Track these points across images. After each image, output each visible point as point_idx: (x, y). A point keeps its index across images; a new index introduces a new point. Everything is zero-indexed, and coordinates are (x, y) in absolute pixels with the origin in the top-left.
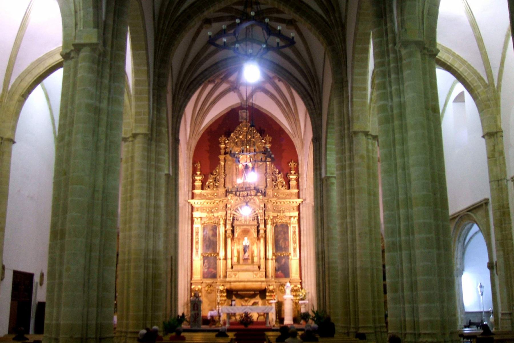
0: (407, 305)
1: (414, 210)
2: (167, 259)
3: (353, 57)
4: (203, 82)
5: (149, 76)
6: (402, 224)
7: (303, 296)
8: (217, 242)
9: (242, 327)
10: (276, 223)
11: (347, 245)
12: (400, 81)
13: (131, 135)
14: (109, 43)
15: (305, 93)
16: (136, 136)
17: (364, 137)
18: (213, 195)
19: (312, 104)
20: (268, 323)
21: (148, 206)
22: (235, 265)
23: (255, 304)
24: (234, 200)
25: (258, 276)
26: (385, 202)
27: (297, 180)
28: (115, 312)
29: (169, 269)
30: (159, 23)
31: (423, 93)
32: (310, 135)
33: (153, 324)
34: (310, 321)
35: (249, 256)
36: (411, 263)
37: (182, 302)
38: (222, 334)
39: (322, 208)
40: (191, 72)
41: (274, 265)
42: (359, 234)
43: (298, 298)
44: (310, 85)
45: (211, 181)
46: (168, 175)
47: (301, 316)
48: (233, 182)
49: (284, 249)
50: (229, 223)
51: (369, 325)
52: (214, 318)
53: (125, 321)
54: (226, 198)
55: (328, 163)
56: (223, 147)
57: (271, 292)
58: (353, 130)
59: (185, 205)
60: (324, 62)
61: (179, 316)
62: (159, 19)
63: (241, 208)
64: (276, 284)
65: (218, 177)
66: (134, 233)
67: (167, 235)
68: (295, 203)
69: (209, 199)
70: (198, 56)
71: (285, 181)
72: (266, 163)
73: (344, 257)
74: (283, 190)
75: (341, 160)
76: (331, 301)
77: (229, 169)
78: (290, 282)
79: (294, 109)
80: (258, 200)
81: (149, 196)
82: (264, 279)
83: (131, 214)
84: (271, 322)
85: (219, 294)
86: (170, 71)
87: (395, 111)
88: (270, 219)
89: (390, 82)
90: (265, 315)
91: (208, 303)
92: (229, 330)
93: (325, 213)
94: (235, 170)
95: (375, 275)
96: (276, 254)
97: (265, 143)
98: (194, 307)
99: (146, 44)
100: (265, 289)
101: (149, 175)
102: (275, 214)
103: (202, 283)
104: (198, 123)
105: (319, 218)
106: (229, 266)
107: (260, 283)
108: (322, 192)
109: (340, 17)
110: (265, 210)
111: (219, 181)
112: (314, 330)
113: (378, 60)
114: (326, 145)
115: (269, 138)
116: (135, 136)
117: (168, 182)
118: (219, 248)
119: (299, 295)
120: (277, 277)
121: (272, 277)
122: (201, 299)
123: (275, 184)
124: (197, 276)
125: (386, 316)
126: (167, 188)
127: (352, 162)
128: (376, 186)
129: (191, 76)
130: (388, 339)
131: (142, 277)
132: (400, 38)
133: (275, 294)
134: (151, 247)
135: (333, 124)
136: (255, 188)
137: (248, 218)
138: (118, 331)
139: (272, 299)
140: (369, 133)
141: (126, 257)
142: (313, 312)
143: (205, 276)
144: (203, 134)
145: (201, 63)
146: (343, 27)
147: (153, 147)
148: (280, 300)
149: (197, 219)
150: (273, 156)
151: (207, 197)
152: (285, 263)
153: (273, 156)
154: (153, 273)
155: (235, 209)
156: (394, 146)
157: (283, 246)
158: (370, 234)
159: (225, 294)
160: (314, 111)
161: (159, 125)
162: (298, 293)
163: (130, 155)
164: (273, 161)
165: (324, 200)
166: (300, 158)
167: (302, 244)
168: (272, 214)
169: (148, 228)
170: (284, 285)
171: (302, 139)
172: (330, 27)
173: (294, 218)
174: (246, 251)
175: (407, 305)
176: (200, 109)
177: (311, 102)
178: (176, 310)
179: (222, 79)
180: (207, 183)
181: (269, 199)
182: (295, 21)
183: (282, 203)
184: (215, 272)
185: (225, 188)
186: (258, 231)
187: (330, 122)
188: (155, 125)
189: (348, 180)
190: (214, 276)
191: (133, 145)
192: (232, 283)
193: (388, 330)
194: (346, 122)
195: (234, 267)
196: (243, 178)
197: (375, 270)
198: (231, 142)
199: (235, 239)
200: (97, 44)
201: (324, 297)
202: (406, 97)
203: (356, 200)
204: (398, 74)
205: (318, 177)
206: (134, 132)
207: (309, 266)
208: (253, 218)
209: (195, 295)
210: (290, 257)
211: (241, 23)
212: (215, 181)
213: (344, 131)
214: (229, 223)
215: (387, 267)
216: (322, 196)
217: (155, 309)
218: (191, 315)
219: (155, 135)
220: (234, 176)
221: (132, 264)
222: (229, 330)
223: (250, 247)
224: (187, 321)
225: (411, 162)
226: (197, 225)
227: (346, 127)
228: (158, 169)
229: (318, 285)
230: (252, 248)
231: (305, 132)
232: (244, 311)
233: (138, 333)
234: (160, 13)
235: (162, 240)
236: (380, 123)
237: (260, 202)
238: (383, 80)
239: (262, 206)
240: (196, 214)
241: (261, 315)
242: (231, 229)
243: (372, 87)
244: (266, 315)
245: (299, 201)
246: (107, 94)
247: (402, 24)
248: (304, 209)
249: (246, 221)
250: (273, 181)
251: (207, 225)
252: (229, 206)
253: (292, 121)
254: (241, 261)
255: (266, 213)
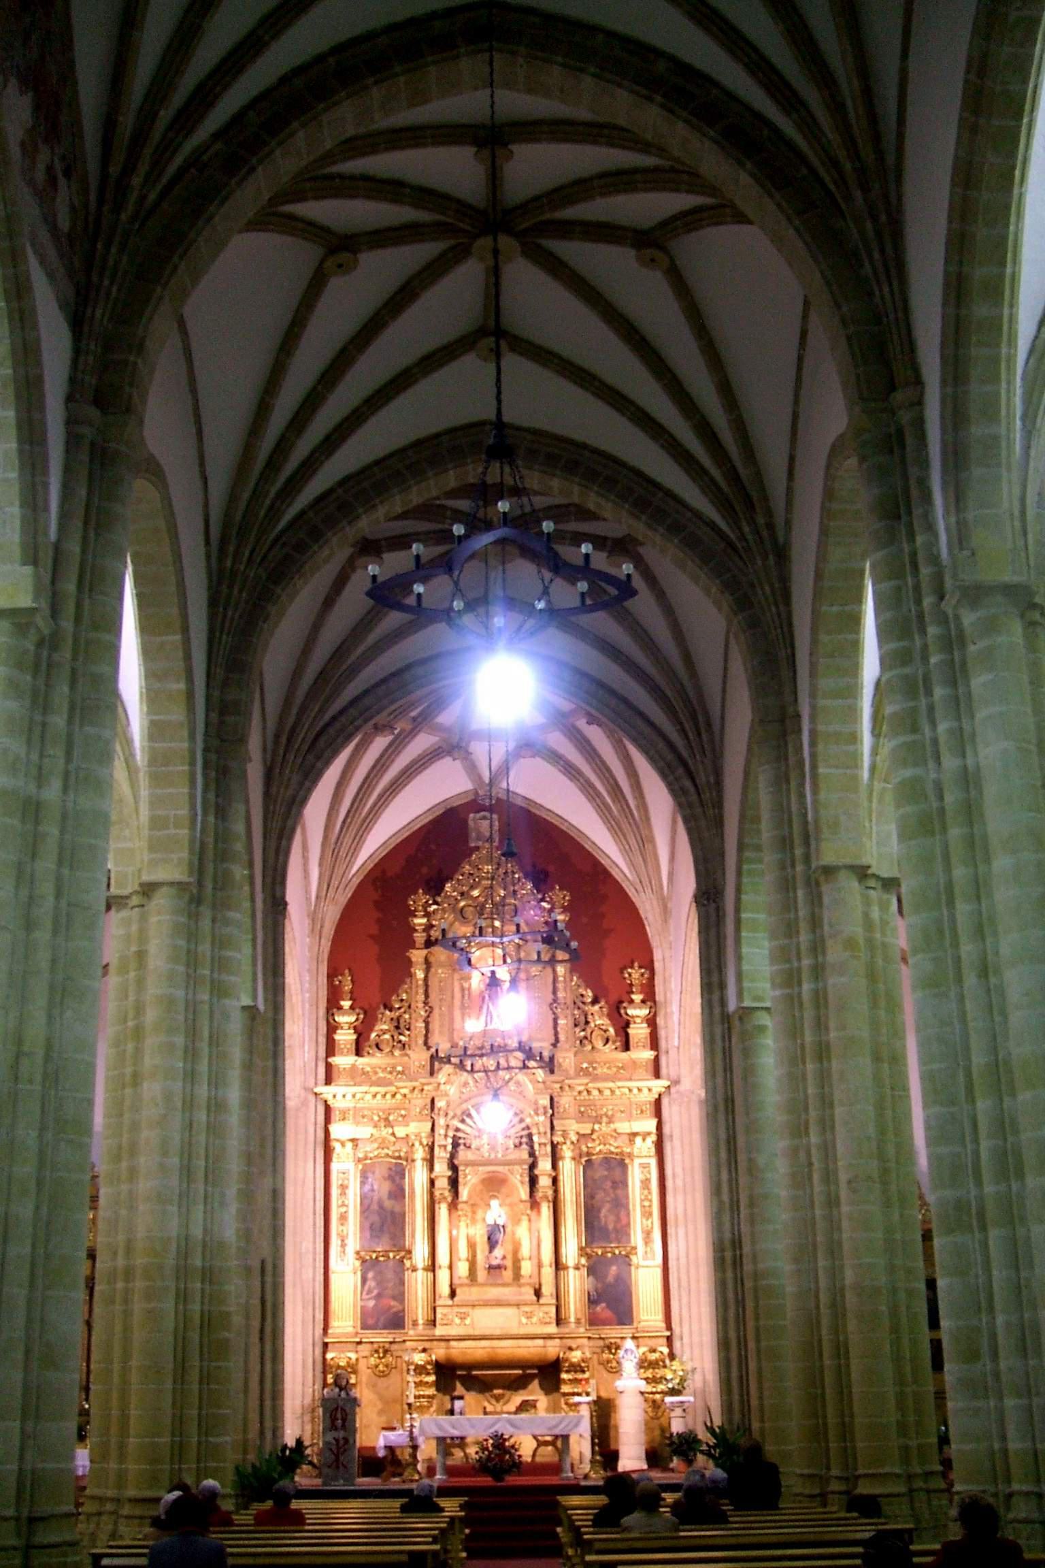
0: (1010, 1402)
1: (1020, 1098)
2: (248, 1270)
3: (814, 641)
4: (357, 729)
5: (191, 709)
6: (985, 1145)
7: (677, 1381)
8: (404, 1215)
9: (486, 1481)
10: (588, 1154)
11: (814, 1218)
12: (960, 705)
13: (137, 888)
14: (70, 608)
15: (670, 757)
16: (154, 890)
17: (855, 884)
18: (391, 1073)
19: (692, 789)
20: (568, 1467)
21: (189, 1104)
22: (461, 1285)
23: (525, 1406)
24: (456, 1084)
25: (534, 1320)
26: (928, 1079)
27: (652, 1022)
28: (82, 1438)
29: (256, 1302)
30: (222, 550)
31: (1034, 741)
32: (688, 884)
33: (201, 1474)
34: (701, 1459)
35: (504, 1257)
36: (1017, 1269)
37: (298, 1402)
38: (421, 1503)
39: (730, 1101)
40: (322, 698)
41: (582, 1284)
42: (849, 1182)
43: (661, 1387)
44: (683, 732)
45: (385, 1027)
46: (251, 1011)
47: (672, 1443)
48: (452, 1030)
49: (613, 1236)
50: (441, 1155)
51: (887, 1469)
52: (398, 1452)
53: (113, 1465)
54: (432, 1080)
55: (745, 967)
56: (420, 925)
57: (576, 1372)
58: (822, 863)
59: (305, 1103)
60: (726, 660)
61: (285, 1447)
62: (224, 541)
63: (478, 1111)
64: (592, 1343)
65: (407, 1016)
66: (144, 1185)
67: (247, 1196)
68: (645, 1091)
69: (378, 1083)
70: (340, 652)
71: (614, 1025)
72: (554, 971)
73: (804, 1252)
74: (609, 1053)
75: (784, 954)
76: (766, 1393)
77: (441, 990)
78: (634, 1338)
79: (638, 807)
80: (531, 1082)
81: (193, 1072)
82: (552, 1329)
83: (135, 1127)
84: (576, 1462)
85: (411, 1379)
86: (257, 695)
87: (949, 798)
88: (568, 1142)
89: (931, 709)
90: (559, 1443)
91: (380, 1405)
92: (445, 1491)
93: (740, 1120)
94: (458, 995)
95: (903, 1309)
96: (589, 1250)
97: (551, 911)
98: (333, 1419)
99: (185, 617)
100: (558, 1359)
101: (192, 1007)
102: (586, 1128)
103: (360, 1343)
104: (342, 853)
105: (723, 1135)
106: (444, 1289)
107: (540, 1342)
108: (727, 1054)
109: (771, 526)
110: (552, 1115)
111: (409, 1029)
112: (714, 1488)
113: (893, 645)
114: (738, 910)
115: (561, 896)
116: (148, 889)
117: (250, 1032)
118: (413, 1236)
119: (663, 1379)
120: (594, 1321)
121: (578, 1321)
122: (356, 1393)
123: (582, 1034)
124: (344, 1322)
125: (944, 1440)
126: (250, 1050)
127: (820, 959)
128: (897, 1033)
129: (322, 711)
130: (954, 1512)
131: (169, 1323)
132: (955, 576)
133: (587, 1375)
134: (197, 1232)
135: (758, 848)
136: (521, 1048)
137: (501, 1139)
138: (93, 1498)
139: (580, 1390)
140: (870, 872)
141: (121, 1262)
142: (711, 1430)
143: (368, 1321)
144: (361, 885)
145: (354, 671)
146: (782, 554)
147: (206, 924)
148: (604, 1394)
149: (343, 1144)
150: (574, 944)
151: (374, 1078)
152: (618, 1278)
153: (574, 944)
154: (202, 1311)
155: (459, 1112)
156: (951, 902)
157: (611, 1227)
158: (885, 1183)
159: (432, 1378)
160: (699, 810)
161: (223, 855)
162: (660, 1373)
163: (134, 949)
164: (577, 962)
165: (738, 1082)
166: (657, 956)
167: (669, 1184)
168: (574, 1127)
169: (187, 1171)
170: (618, 1348)
171: (663, 898)
172: (741, 557)
173: (644, 1140)
174: (497, 1242)
175: (1010, 1402)
176: (349, 812)
177: (688, 784)
178: (277, 1431)
179: (414, 719)
180: (373, 1035)
181: (567, 1081)
182: (636, 542)
183: (607, 1092)
184: (400, 1308)
185: (428, 1048)
186: (533, 1181)
187: (746, 840)
188: (210, 854)
189: (809, 1014)
190: (396, 1322)
191: (143, 919)
192: (453, 1343)
193: (951, 1485)
194: (797, 840)
195: (458, 1291)
196: (483, 1018)
197: (902, 1295)
198: (444, 910)
199: (460, 1206)
200: (31, 611)
201: (743, 1380)
202: (981, 755)
203: (835, 1076)
204: (954, 684)
205: (717, 1011)
206: (146, 878)
207: (693, 1286)
208: (517, 1141)
209: (336, 1383)
210: (634, 1259)
211: (467, 536)
212: (397, 1027)
213: (793, 866)
214: (441, 1155)
215: (941, 1283)
216: (728, 1068)
217: (208, 1426)
218: (326, 1443)
219: (209, 885)
220: (457, 1014)
221: (139, 1284)
222: (445, 1491)
223: (508, 1229)
224: (311, 1463)
225: (1005, 950)
226: (343, 1163)
227: (798, 852)
228: (220, 990)
229: (723, 1345)
230: (513, 1233)
231: (671, 874)
232: (492, 1430)
233: (157, 1500)
234: (226, 524)
235: (233, 1208)
236: (903, 836)
237: (538, 1092)
238: (912, 704)
239: (545, 1102)
240: (338, 1130)
241: (546, 1443)
242: (450, 1173)
243: (876, 733)
244: (561, 1441)
245: (659, 1085)
246: (62, 761)
247: (961, 537)
248: (675, 1108)
249: (493, 1148)
250: (576, 1025)
251: (373, 1164)
252: (440, 1104)
253: (633, 842)
254: (482, 1275)
255: (555, 1122)
